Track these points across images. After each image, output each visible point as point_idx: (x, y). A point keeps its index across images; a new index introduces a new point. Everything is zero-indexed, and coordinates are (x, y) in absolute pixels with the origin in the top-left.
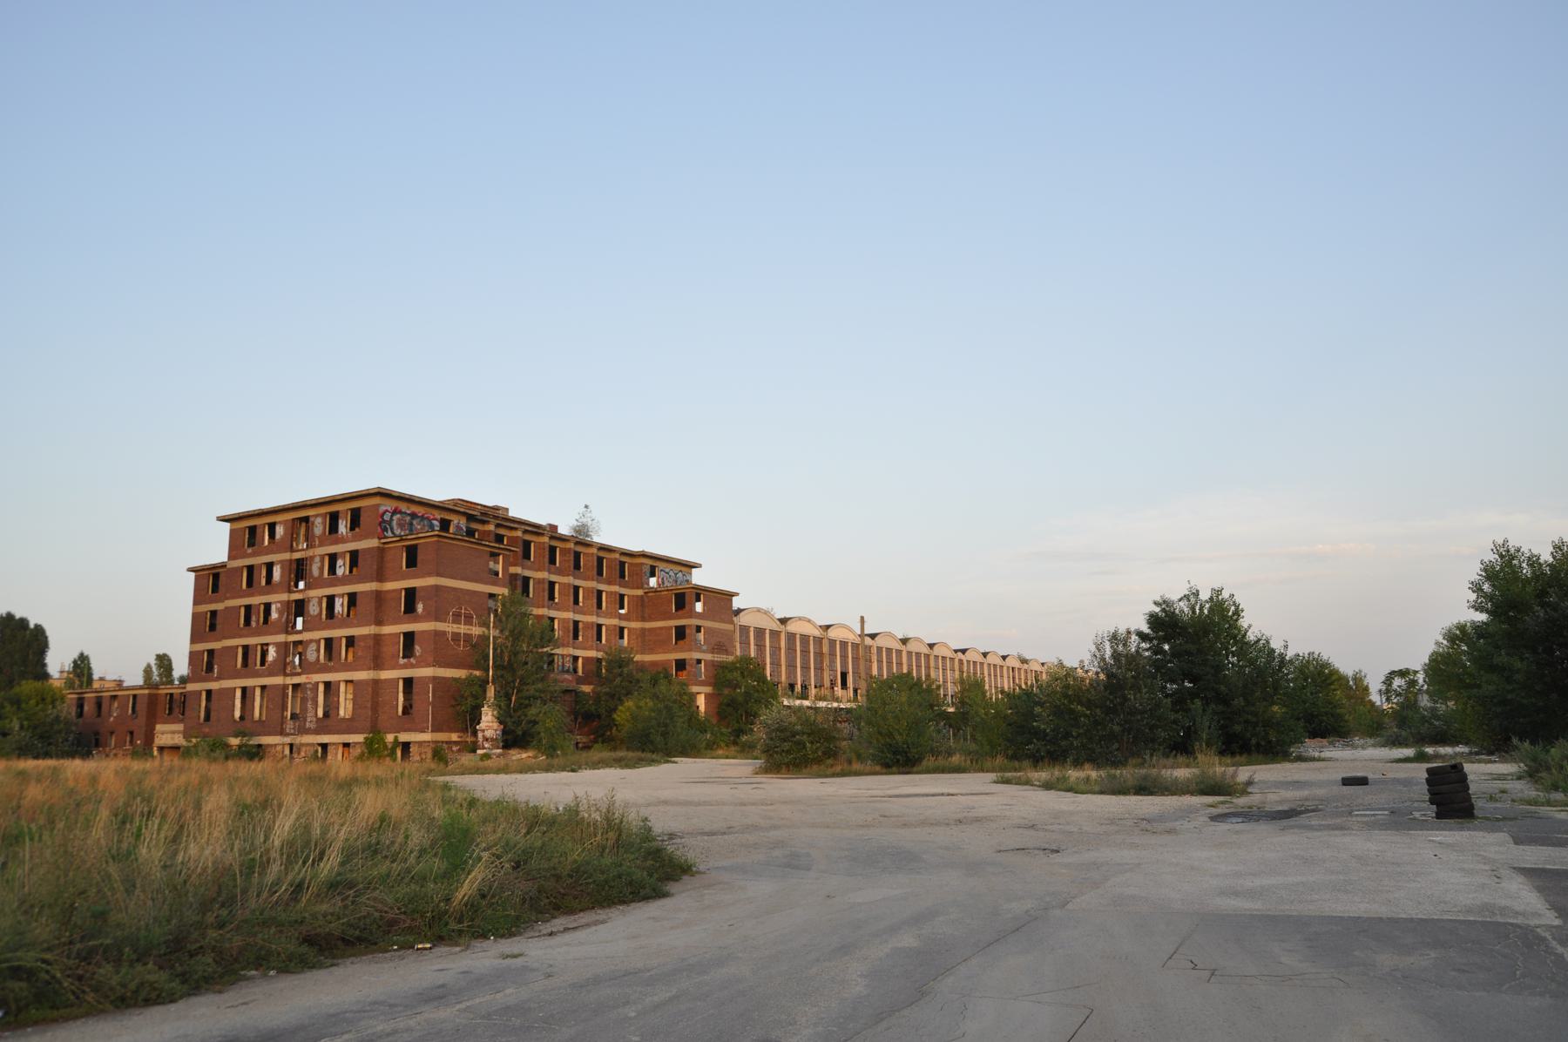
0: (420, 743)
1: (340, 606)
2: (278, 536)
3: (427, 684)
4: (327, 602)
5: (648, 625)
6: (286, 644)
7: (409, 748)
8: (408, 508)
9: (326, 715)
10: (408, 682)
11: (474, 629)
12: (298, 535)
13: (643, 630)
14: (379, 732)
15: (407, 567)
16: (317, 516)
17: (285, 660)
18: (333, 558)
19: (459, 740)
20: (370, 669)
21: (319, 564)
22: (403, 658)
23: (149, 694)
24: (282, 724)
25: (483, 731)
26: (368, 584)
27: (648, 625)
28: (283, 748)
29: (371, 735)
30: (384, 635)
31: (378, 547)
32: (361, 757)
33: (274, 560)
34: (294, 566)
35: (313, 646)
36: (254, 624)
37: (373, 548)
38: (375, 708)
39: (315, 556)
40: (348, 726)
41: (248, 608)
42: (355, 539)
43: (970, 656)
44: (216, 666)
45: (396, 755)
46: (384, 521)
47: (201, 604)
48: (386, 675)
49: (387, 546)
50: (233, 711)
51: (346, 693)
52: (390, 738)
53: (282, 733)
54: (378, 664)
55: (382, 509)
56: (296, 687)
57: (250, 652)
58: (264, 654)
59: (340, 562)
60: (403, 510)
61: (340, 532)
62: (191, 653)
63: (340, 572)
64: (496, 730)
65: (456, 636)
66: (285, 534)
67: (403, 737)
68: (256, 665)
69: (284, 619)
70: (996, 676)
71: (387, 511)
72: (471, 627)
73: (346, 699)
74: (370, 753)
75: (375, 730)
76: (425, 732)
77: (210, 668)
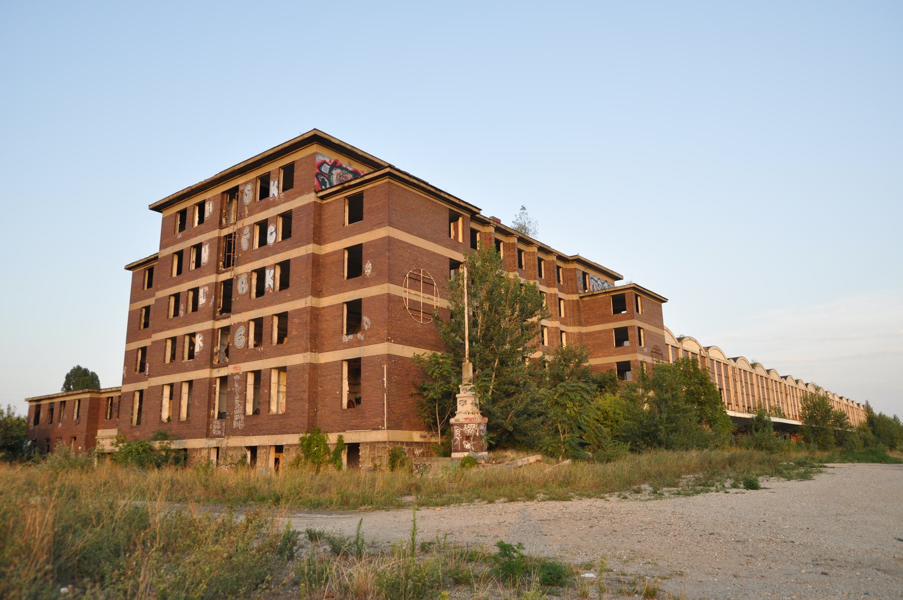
0: (373, 445)
1: (271, 279)
2: (207, 215)
3: (380, 365)
4: (258, 279)
5: (585, 330)
6: (213, 331)
7: (358, 451)
8: (350, 164)
9: (256, 412)
10: (355, 366)
11: (435, 298)
12: (228, 211)
13: (580, 334)
14: (319, 431)
15: (349, 223)
16: (246, 183)
17: (212, 350)
18: (263, 226)
19: (422, 440)
20: (306, 351)
21: (248, 236)
22: (347, 334)
23: (90, 398)
24: (208, 424)
25: (461, 425)
26: (304, 248)
27: (585, 330)
28: (209, 453)
29: (309, 435)
30: (324, 308)
31: (315, 202)
32: (296, 463)
33: (203, 240)
34: (223, 244)
35: (241, 330)
36: (181, 313)
37: (309, 204)
38: (313, 399)
40: (281, 425)
41: (177, 296)
42: (287, 199)
44: (148, 364)
45: (341, 460)
46: (322, 173)
47: (137, 302)
48: (326, 358)
50: (161, 411)
51: (279, 385)
52: (332, 438)
53: (208, 435)
54: (316, 344)
55: (319, 159)
56: (224, 380)
57: (178, 344)
58: (192, 344)
59: (271, 229)
60: (344, 166)
61: (271, 195)
62: (126, 352)
63: (271, 239)
64: (479, 424)
65: (415, 306)
66: (214, 210)
67: (350, 437)
68: (183, 358)
69: (211, 304)
71: (324, 162)
72: (431, 297)
73: (278, 392)
74: (307, 457)
75: (314, 428)
76: (378, 429)
77: (142, 369)
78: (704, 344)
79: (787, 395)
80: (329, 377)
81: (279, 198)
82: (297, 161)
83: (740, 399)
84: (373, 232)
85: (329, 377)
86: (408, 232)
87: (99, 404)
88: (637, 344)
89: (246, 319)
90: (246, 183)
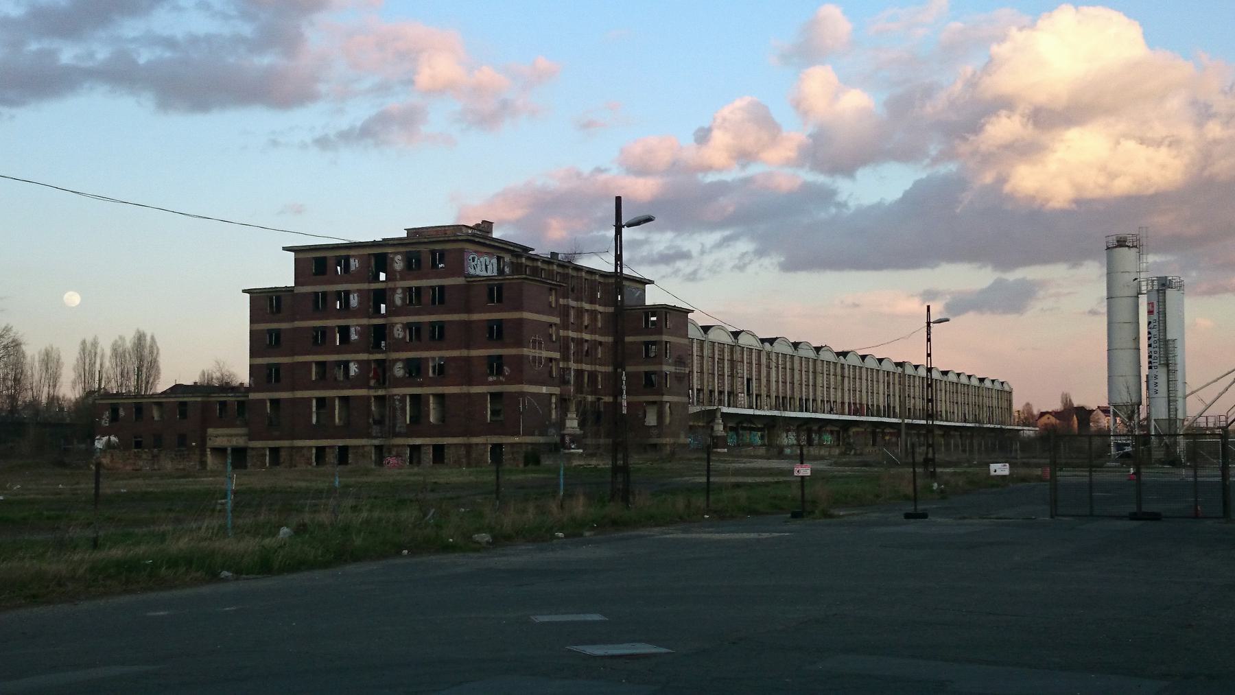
6: (368, 362)
39: (397, 288)
43: (777, 347)
49: (470, 283)
53: (369, 436)
70: (872, 381)
83: (797, 376)
88: (664, 357)
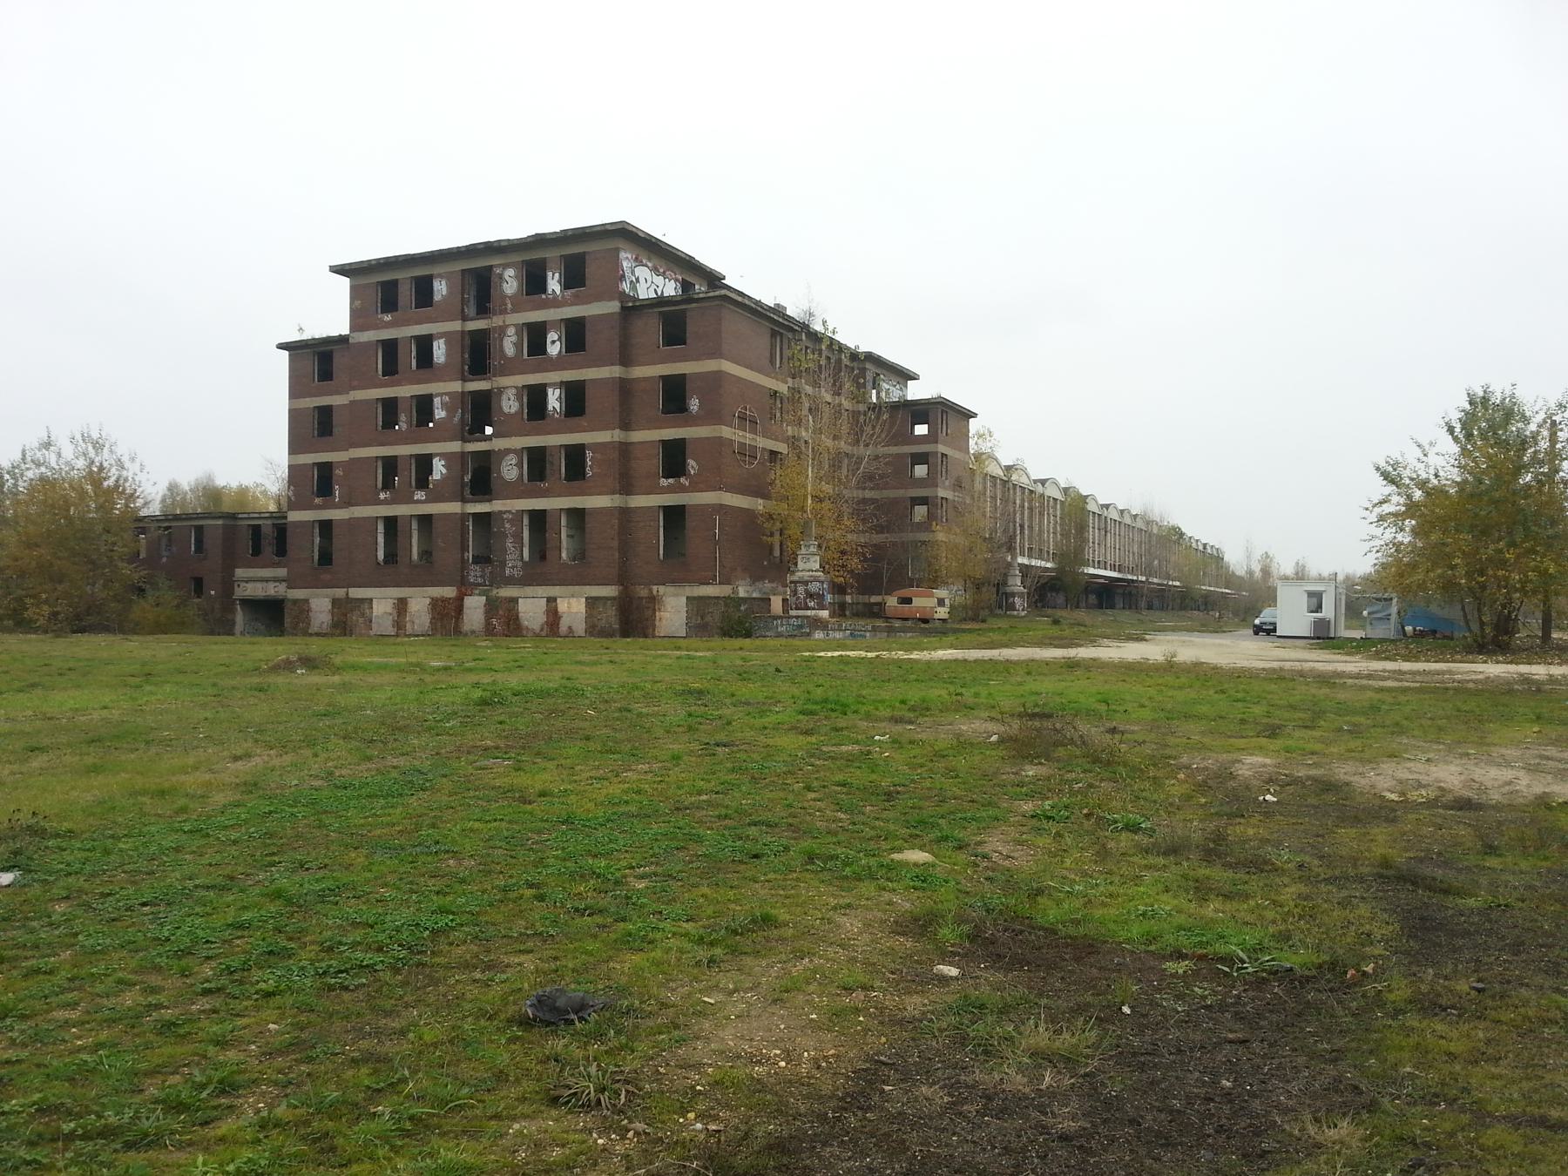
1: (554, 400)
76: (709, 584)
78: (1005, 462)
79: (1106, 532)
80: (642, 524)
81: (562, 297)
82: (588, 252)
84: (700, 362)
85: (642, 524)
86: (735, 363)
87: (1150, 607)
89: (519, 446)
90: (505, 266)
